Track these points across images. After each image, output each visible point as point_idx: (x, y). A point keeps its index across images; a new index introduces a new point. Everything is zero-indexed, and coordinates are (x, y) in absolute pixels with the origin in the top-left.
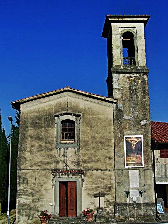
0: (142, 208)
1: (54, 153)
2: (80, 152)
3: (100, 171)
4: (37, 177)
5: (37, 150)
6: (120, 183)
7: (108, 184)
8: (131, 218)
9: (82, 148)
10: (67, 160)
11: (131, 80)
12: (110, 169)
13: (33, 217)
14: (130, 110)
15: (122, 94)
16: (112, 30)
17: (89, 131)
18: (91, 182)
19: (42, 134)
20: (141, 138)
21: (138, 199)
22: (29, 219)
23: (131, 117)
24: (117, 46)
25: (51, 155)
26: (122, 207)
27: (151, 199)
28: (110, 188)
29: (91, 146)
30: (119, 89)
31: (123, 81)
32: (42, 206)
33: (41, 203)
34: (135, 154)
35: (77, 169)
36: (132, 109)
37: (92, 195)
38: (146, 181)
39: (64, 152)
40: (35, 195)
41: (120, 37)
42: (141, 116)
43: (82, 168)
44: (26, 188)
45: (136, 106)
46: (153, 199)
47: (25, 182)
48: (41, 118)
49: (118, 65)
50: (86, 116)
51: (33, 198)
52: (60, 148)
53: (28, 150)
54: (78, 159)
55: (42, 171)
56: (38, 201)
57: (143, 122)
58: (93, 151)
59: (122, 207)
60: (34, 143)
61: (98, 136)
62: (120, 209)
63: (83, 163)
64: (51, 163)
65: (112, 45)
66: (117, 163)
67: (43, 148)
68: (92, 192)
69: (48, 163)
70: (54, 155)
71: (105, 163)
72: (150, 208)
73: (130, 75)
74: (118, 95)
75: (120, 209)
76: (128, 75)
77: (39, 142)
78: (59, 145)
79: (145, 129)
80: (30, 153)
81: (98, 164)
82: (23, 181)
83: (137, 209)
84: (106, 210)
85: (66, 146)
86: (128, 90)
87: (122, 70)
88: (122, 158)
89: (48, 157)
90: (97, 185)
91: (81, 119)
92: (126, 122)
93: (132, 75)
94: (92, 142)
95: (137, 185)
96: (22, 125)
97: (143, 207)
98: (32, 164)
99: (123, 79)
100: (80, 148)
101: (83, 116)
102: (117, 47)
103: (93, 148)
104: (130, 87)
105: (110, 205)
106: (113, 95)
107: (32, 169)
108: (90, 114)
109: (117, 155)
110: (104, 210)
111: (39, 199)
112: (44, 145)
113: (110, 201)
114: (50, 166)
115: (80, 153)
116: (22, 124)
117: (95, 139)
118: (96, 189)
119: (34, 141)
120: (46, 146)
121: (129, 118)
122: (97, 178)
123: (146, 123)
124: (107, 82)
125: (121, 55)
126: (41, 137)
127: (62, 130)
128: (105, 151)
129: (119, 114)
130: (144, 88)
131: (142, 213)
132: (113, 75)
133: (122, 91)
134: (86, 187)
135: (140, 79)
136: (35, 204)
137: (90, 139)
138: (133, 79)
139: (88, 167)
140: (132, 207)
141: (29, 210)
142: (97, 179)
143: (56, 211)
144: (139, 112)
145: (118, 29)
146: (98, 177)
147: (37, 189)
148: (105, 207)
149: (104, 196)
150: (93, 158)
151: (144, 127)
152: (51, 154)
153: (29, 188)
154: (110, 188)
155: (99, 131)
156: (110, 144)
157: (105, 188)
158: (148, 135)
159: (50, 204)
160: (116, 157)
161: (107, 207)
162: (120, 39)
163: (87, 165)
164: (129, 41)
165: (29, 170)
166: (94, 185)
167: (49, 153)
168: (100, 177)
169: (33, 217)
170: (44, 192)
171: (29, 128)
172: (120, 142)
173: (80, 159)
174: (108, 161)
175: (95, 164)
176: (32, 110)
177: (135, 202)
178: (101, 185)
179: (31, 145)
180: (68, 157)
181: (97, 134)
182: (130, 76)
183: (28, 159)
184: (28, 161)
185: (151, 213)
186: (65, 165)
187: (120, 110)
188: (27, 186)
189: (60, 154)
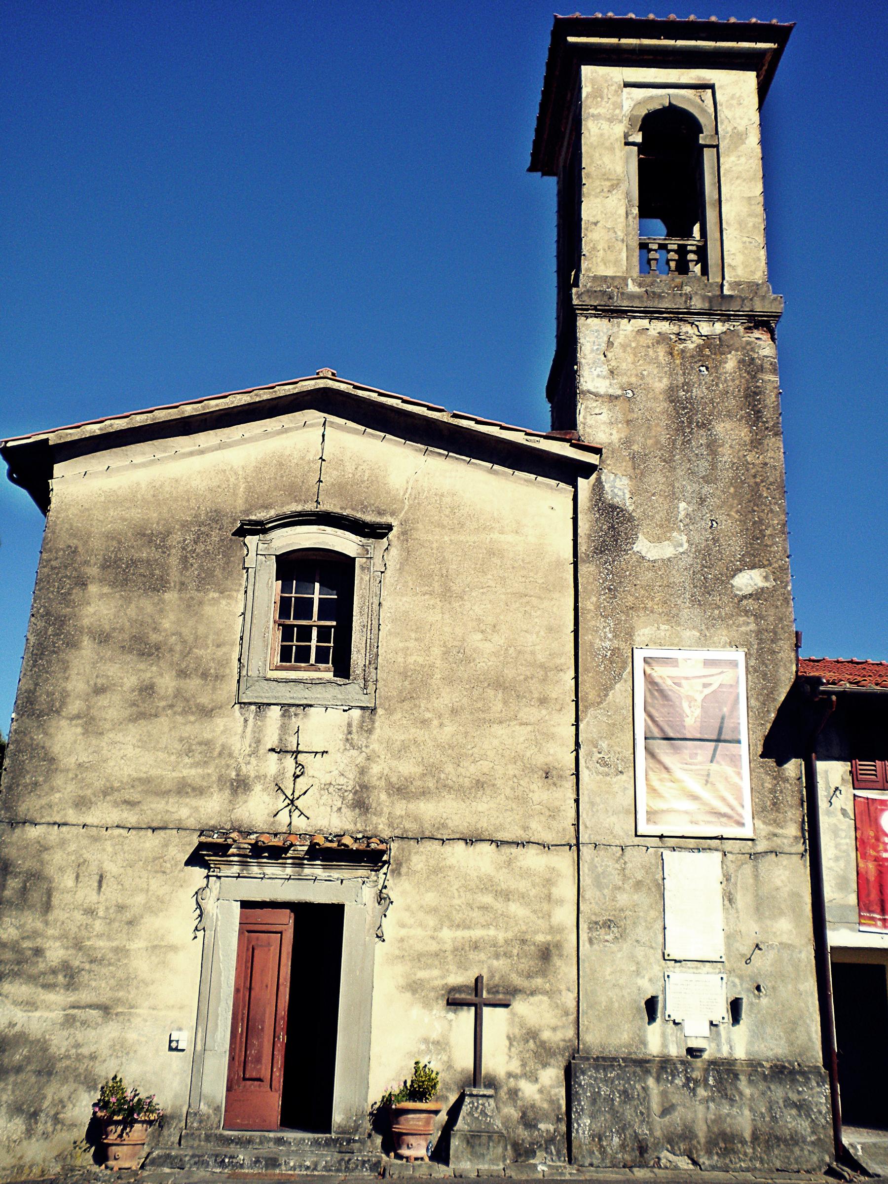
0: (741, 1094)
1: (223, 732)
2: (377, 732)
3: (486, 847)
4: (111, 868)
5: (128, 712)
6: (608, 925)
7: (536, 932)
8: (671, 1157)
9: (390, 711)
10: (296, 777)
11: (683, 351)
12: (548, 837)
13: (56, 1120)
14: (672, 511)
15: (628, 422)
16: (584, 95)
17: (434, 617)
18: (434, 910)
19: (166, 624)
20: (734, 664)
21: (718, 1034)
22: (29, 1133)
23: (675, 547)
24: (608, 179)
25: (207, 743)
26: (618, 1077)
27: (802, 1038)
28: (546, 954)
29: (447, 698)
30: (612, 398)
31: (635, 355)
32: (121, 1048)
33: (115, 1034)
34: (700, 758)
35: (350, 827)
36: (682, 505)
37: (432, 994)
38: (769, 922)
39: (284, 728)
40: (85, 977)
41: (626, 136)
42: (735, 546)
43: (381, 826)
44: (35, 934)
45: (707, 489)
46: (810, 1039)
47: (35, 896)
48: (169, 533)
49: (610, 272)
50: (421, 534)
51: (72, 998)
52: (261, 706)
53: (75, 712)
54: (363, 771)
55: (142, 832)
56: (100, 1020)
57: (748, 581)
58: (449, 729)
59: (618, 1077)
60: (113, 670)
61: (487, 645)
62: (605, 1090)
63: (389, 795)
64: (200, 791)
65: (580, 169)
66: (592, 804)
67: (162, 704)
68: (436, 972)
69: (184, 789)
70: (223, 747)
71: (522, 800)
72: (794, 1097)
73: (675, 329)
74: (603, 427)
75: (605, 1090)
76: (664, 326)
77: (142, 666)
78: (257, 687)
79: (758, 617)
80: (79, 730)
81: (480, 809)
82: (24, 891)
83: (713, 1100)
84: (514, 1093)
85: (299, 695)
86: (662, 405)
87: (632, 296)
88: (623, 777)
89: (189, 752)
90: (467, 934)
91: (394, 551)
92: (650, 574)
93: (686, 328)
94: (449, 680)
95: (712, 961)
96: (53, 568)
97: (750, 1082)
98: (89, 792)
99: (633, 345)
100: (380, 711)
101: (404, 533)
102: (608, 183)
103: (454, 712)
104: (671, 394)
105: (545, 1065)
106: (580, 427)
107: (82, 820)
108: (443, 527)
109: (590, 754)
110: (503, 1093)
111: (105, 1009)
112: (167, 683)
113: (546, 1035)
114: (196, 809)
115: (375, 736)
116: (53, 563)
117: (468, 660)
118: (461, 953)
119: (111, 660)
120: (178, 694)
121: (666, 551)
122: (467, 888)
123: (761, 583)
124: (550, 396)
125: (627, 226)
126: (154, 637)
127: (284, 606)
128: (522, 733)
129: (613, 530)
130: (752, 397)
131: (743, 1121)
132: (581, 321)
133: (632, 411)
134: (402, 940)
135: (731, 348)
136: (80, 1037)
137: (438, 663)
138: (692, 346)
139: (416, 819)
140: (679, 1081)
141: (39, 1073)
142: (469, 895)
143: (207, 1088)
144: (728, 523)
145: (613, 103)
146: (473, 885)
147: (101, 943)
148: (510, 1075)
149: (506, 1006)
150: (449, 768)
151: (750, 604)
152: (207, 736)
153: (56, 938)
154: (546, 954)
155: (490, 620)
156: (554, 696)
157: (515, 952)
158: (774, 652)
159: (168, 1014)
160: (584, 773)
161: (524, 1075)
162: (627, 144)
163: (412, 806)
164: (672, 155)
165: (64, 829)
166: (447, 934)
167: (192, 729)
168: (487, 885)
169: (56, 1120)
170: (141, 965)
171: (93, 589)
172: (612, 688)
173: (375, 769)
174: (539, 794)
175: (464, 805)
176: (120, 493)
177: (693, 1052)
178: (492, 932)
179: (92, 683)
180: (301, 757)
181: (480, 636)
182: (678, 334)
183: (69, 761)
184: (68, 771)
185: (803, 1126)
186: (281, 803)
187: (613, 507)
188: (39, 925)
189: (258, 741)
